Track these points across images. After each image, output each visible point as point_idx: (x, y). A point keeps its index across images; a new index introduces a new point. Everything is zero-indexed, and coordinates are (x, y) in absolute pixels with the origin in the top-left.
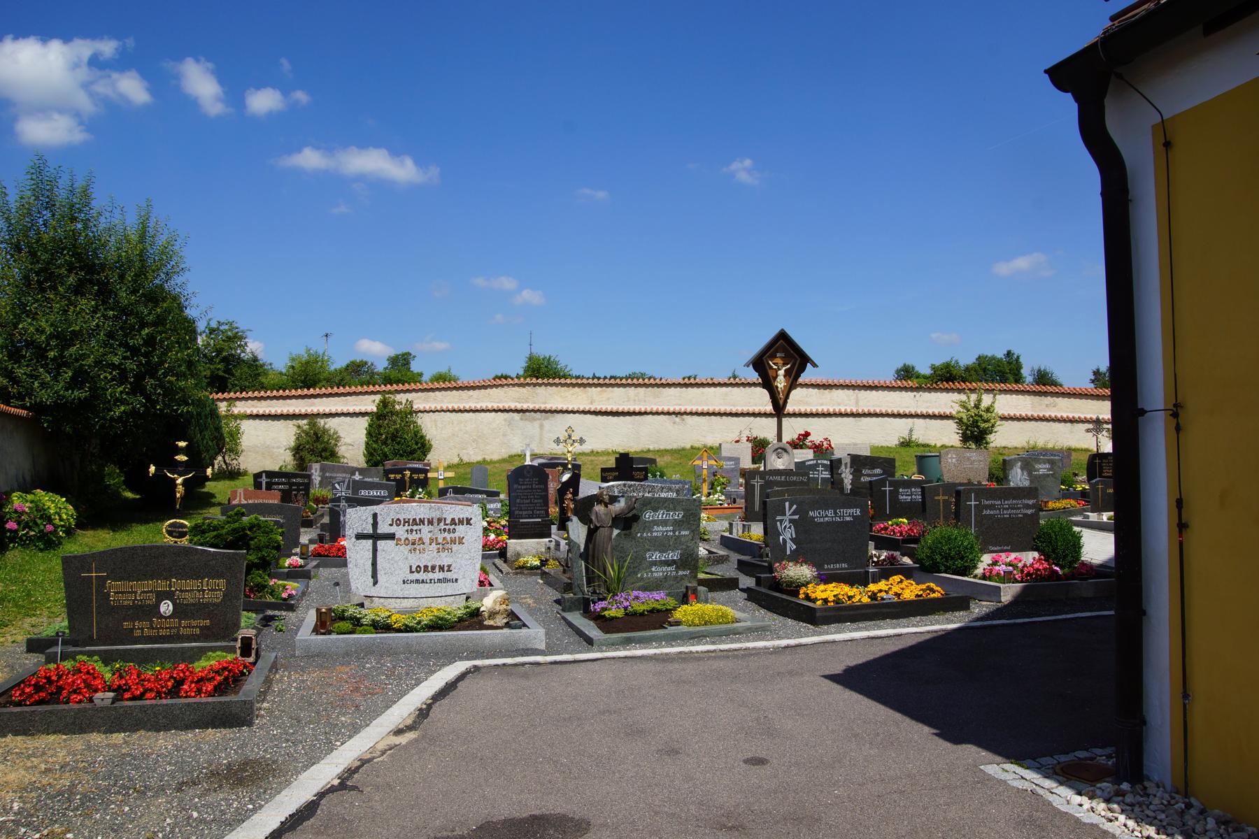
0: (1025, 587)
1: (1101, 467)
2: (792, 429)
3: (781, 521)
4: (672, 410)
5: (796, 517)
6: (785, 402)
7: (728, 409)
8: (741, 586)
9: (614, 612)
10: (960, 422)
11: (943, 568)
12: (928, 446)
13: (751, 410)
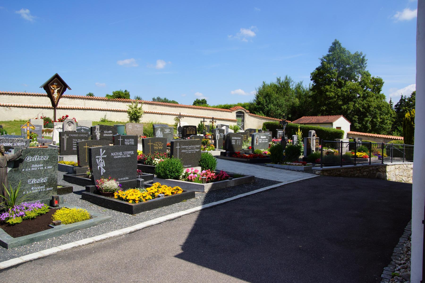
0: (213, 185)
1: (186, 131)
2: (60, 114)
3: (98, 158)
4: (5, 104)
5: (105, 156)
6: (57, 103)
7: (31, 105)
8: (74, 191)
9: (14, 220)
10: (129, 113)
11: (169, 177)
12: (112, 122)
13: (41, 106)
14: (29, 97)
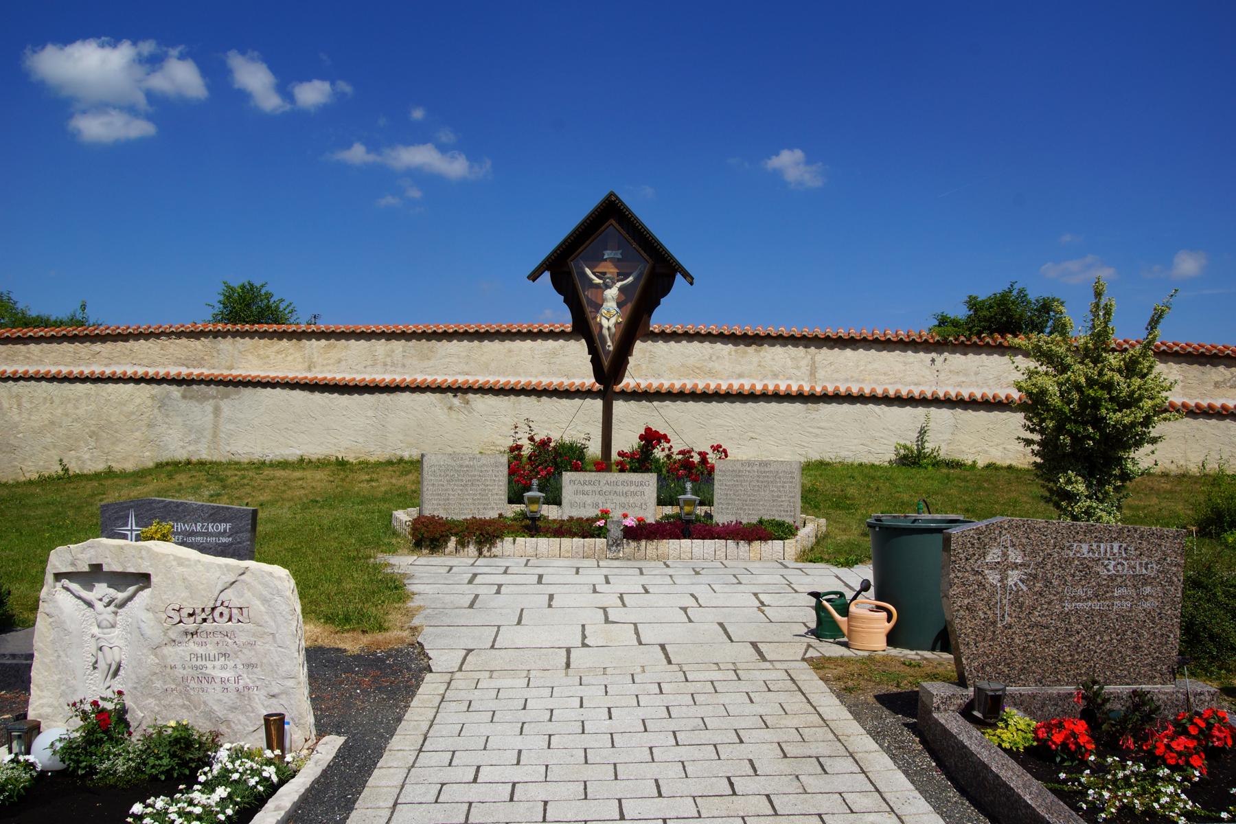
12: (957, 465)
14: (551, 344)
